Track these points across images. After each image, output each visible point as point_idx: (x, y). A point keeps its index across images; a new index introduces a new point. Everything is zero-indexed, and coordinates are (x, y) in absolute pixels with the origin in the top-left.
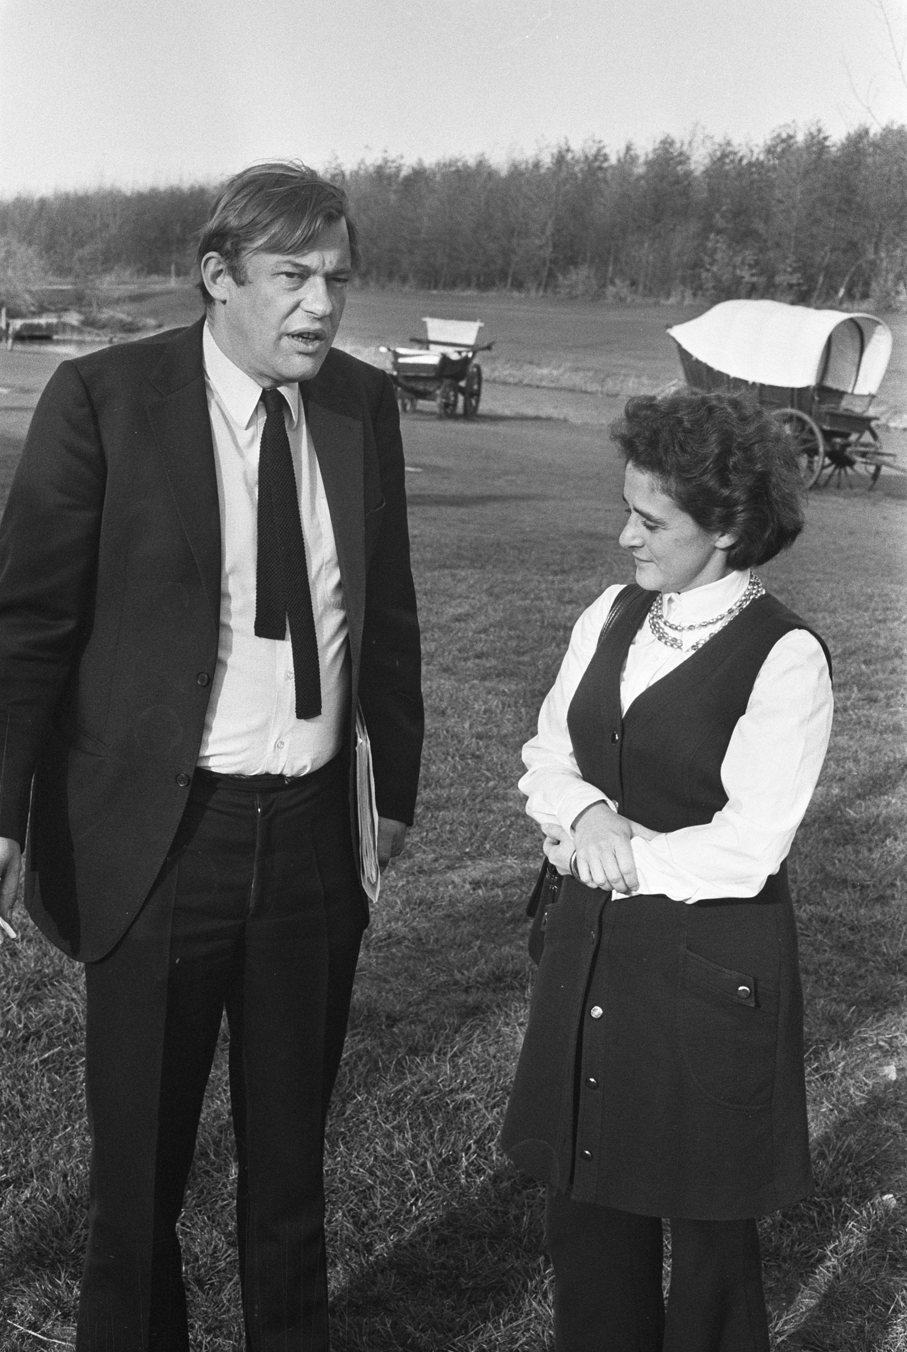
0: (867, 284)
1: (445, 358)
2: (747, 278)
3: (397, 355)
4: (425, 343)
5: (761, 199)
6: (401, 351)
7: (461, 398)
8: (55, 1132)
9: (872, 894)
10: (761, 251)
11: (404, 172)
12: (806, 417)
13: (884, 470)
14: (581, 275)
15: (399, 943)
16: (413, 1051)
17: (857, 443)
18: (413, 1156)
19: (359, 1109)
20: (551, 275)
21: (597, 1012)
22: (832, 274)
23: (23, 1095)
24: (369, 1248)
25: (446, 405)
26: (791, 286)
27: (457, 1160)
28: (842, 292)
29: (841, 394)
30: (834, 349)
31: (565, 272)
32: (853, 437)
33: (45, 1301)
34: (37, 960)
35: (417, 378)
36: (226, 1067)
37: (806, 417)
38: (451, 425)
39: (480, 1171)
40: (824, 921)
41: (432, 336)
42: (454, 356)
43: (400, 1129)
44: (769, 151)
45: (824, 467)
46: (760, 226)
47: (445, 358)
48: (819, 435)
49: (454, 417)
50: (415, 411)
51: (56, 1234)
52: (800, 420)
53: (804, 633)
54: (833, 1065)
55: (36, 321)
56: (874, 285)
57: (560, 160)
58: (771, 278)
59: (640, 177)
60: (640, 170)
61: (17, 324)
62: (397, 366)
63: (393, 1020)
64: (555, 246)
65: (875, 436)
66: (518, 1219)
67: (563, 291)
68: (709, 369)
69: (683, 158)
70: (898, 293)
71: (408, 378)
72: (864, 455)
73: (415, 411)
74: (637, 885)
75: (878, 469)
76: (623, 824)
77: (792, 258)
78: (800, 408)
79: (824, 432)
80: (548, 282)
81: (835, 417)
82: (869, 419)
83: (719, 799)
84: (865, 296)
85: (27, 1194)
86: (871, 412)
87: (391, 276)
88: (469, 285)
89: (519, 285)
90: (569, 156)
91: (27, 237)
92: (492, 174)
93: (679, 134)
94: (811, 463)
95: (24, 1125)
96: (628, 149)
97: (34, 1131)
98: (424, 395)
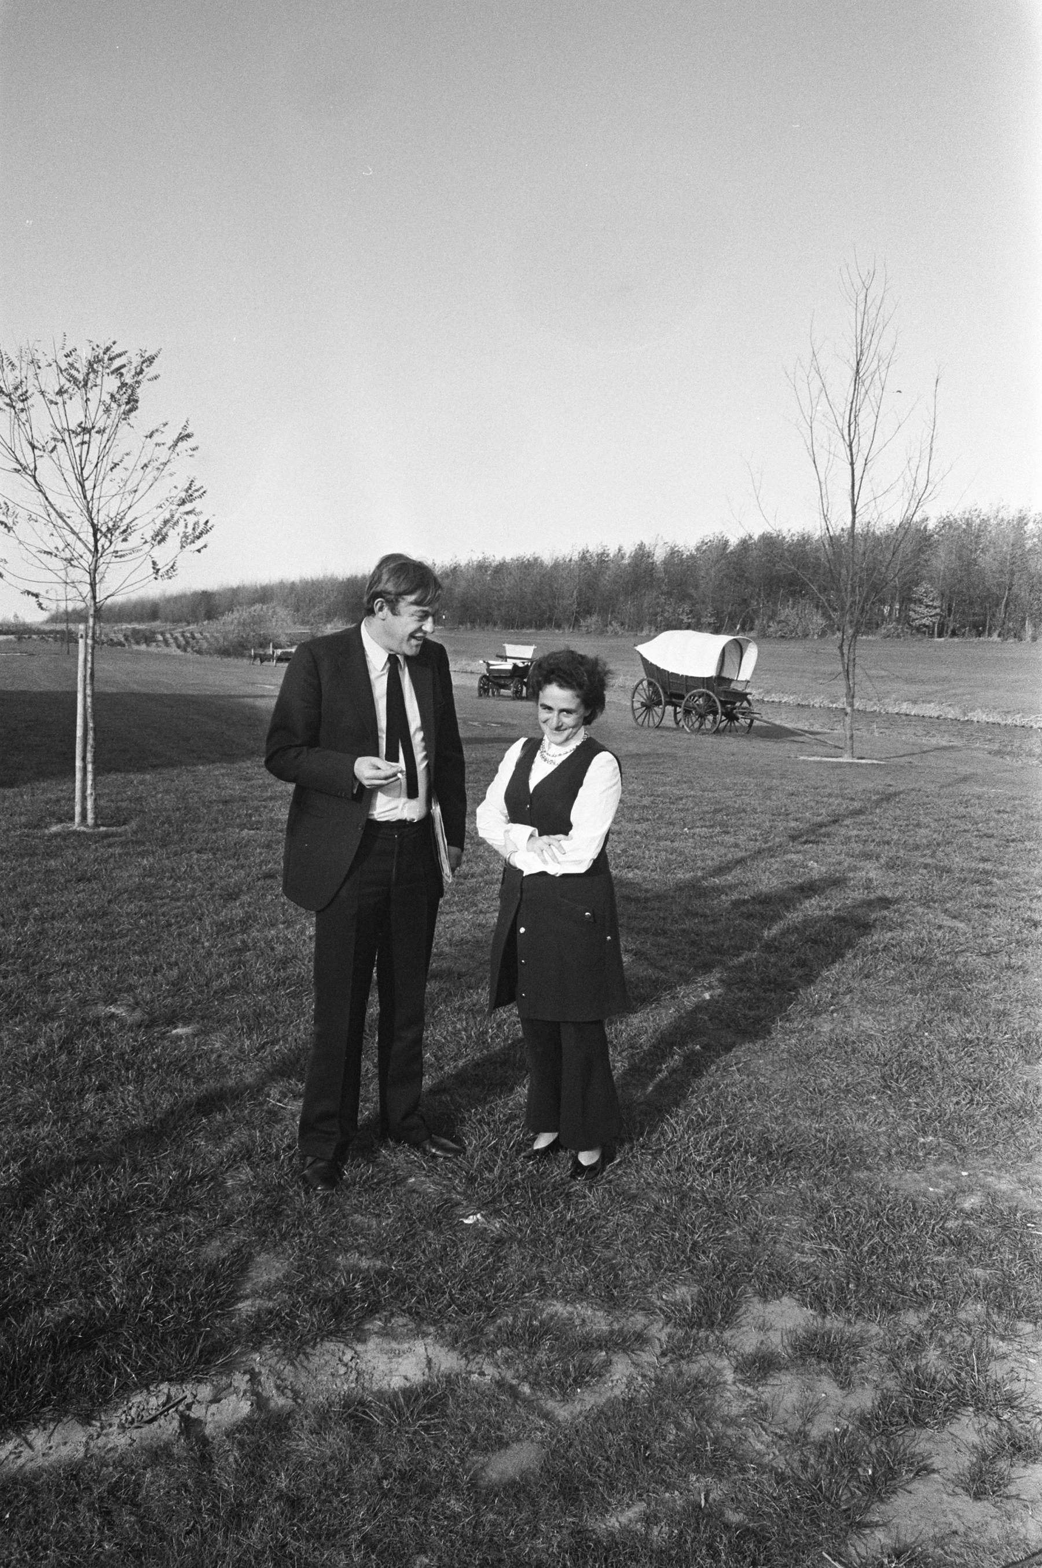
0: (752, 622)
1: (515, 666)
2: (685, 620)
3: (489, 665)
4: (505, 658)
6: (491, 662)
7: (525, 688)
8: (292, 1022)
9: (709, 919)
10: (693, 605)
11: (496, 563)
12: (711, 693)
13: (756, 723)
14: (593, 620)
15: (467, 943)
16: (469, 987)
17: (740, 707)
18: (465, 1030)
19: (441, 1012)
20: (577, 620)
21: (522, 930)
22: (732, 617)
23: (276, 1008)
24: (442, 1068)
25: (516, 692)
26: (710, 624)
27: (487, 1032)
28: (738, 627)
29: (730, 681)
31: (585, 618)
32: (738, 704)
33: (285, 1090)
34: (284, 951)
35: (500, 677)
36: (377, 995)
37: (711, 693)
38: (519, 703)
39: (497, 1037)
40: (684, 931)
41: (508, 654)
42: (521, 665)
43: (460, 1020)
44: (698, 549)
45: (721, 722)
46: (692, 591)
47: (515, 666)
48: (718, 704)
49: (521, 698)
50: (499, 695)
51: (291, 1063)
52: (708, 695)
53: (607, 753)
54: (679, 993)
55: (289, 650)
56: (757, 622)
57: (583, 558)
58: (699, 619)
59: (626, 566)
60: (626, 561)
61: (279, 652)
62: (488, 670)
63: (460, 976)
64: (579, 604)
65: (750, 704)
66: (514, 1056)
67: (584, 629)
68: (658, 668)
69: (649, 555)
70: (769, 627)
71: (495, 677)
72: (743, 714)
73: (499, 695)
75: (752, 722)
77: (710, 609)
78: (708, 688)
79: (721, 701)
80: (575, 624)
82: (747, 694)
83: (570, 826)
84: (751, 629)
85: (277, 1047)
86: (748, 691)
87: (487, 622)
88: (531, 627)
89: (558, 626)
90: (588, 555)
91: (285, 603)
92: (542, 564)
93: (648, 543)
94: (715, 718)
95: (276, 1020)
96: (620, 550)
97: (281, 1022)
98: (505, 687)
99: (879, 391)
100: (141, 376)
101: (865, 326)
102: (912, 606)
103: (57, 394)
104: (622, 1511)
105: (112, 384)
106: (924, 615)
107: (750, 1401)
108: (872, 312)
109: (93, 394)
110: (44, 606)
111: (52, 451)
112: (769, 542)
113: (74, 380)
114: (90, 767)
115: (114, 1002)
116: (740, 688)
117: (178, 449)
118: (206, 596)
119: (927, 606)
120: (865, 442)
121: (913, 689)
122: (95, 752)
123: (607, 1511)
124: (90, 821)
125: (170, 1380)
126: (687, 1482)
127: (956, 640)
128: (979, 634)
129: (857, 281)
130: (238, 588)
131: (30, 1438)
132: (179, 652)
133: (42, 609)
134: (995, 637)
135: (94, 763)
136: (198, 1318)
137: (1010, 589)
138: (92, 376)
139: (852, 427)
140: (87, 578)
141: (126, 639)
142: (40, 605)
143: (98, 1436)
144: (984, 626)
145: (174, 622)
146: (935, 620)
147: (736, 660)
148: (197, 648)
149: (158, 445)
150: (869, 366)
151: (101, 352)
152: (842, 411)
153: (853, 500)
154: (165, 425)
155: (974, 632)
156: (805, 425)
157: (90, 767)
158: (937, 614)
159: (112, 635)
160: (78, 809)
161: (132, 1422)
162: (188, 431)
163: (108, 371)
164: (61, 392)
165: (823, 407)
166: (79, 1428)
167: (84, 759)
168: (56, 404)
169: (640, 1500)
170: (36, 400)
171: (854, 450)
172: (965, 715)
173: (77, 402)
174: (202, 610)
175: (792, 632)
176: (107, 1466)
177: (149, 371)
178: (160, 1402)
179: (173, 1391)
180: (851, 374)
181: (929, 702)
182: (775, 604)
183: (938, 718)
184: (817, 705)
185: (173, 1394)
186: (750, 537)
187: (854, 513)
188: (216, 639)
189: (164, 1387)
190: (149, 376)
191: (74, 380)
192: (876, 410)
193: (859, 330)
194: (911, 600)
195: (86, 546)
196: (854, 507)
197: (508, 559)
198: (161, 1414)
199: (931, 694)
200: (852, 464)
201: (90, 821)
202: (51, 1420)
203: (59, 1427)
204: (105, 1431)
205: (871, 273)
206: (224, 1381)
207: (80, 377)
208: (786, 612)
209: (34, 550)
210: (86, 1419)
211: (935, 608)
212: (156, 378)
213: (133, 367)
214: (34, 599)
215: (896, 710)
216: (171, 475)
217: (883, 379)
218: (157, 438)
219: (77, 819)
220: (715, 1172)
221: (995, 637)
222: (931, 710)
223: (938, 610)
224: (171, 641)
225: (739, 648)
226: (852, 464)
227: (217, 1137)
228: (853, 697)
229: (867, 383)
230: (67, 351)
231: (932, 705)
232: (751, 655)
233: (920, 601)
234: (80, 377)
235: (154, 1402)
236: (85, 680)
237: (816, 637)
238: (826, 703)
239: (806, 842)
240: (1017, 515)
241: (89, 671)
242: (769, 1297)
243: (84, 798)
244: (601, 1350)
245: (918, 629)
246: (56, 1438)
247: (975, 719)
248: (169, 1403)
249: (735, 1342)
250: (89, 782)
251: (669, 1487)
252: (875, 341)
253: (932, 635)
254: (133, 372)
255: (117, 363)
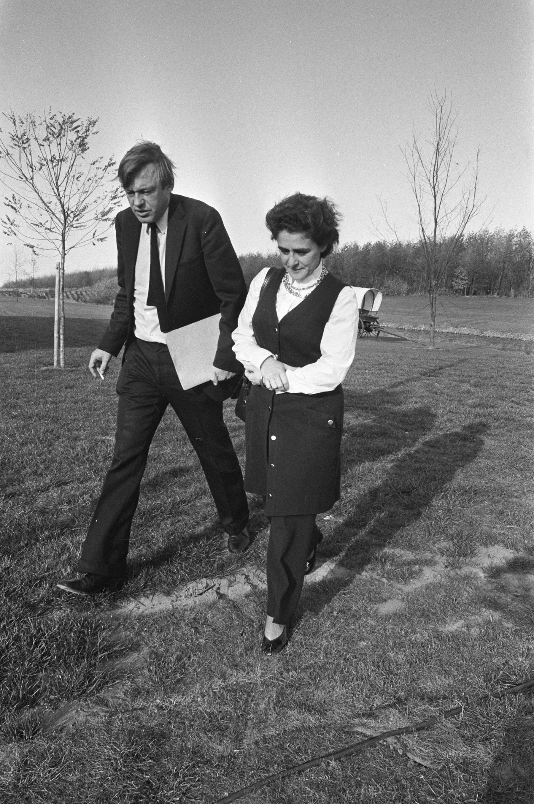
5: (341, 264)
29: (368, 311)
30: (366, 299)
32: (372, 323)
46: (341, 271)
65: (377, 323)
72: (375, 328)
74: (288, 389)
76: (280, 364)
81: (367, 317)
86: (377, 316)
99: (449, 158)
100: (88, 133)
101: (441, 125)
102: (454, 279)
103: (44, 140)
104: (453, 624)
105: (72, 136)
106: (461, 284)
107: (495, 584)
108: (445, 117)
109: (63, 141)
110: (36, 253)
111: (40, 170)
112: (380, 247)
113: (53, 134)
114: (62, 337)
115: (107, 434)
116: (373, 315)
117: (108, 170)
118: (87, 273)
119: (461, 279)
120: (441, 186)
121: (455, 320)
122: (64, 329)
123: (446, 623)
124: (62, 365)
125: (206, 577)
126: (481, 612)
127: (476, 296)
128: (488, 293)
129: (437, 104)
130: (103, 270)
131: (142, 601)
132: (74, 302)
133: (35, 254)
134: (495, 295)
135: (64, 334)
136: (208, 555)
137: (503, 271)
138: (63, 131)
139: (435, 178)
140: (60, 238)
141: (47, 295)
142: (34, 252)
143: (177, 601)
144: (490, 289)
145: (70, 287)
146: (466, 286)
147: (371, 302)
148: (84, 299)
149: (98, 168)
150: (444, 145)
151: (67, 118)
152: (429, 169)
153: (435, 215)
154: (101, 158)
155: (485, 292)
156: (411, 176)
157: (62, 337)
158: (467, 283)
159: (40, 294)
160: (55, 358)
161: (191, 595)
162: (113, 161)
163: (70, 129)
164: (47, 139)
165: (420, 168)
166: (165, 598)
167: (59, 332)
168: (43, 146)
169: (461, 619)
170: (32, 142)
171: (436, 190)
172: (482, 333)
173: (54, 145)
174: (84, 281)
175: (392, 292)
176: (187, 611)
177: (93, 129)
178: (204, 586)
179: (209, 581)
180: (434, 149)
181: (464, 327)
182: (383, 278)
183: (468, 334)
184: (406, 328)
185: (209, 583)
186: (370, 244)
187: (436, 222)
188: (94, 295)
189: (204, 580)
190: (93, 132)
191: (53, 134)
192: (447, 168)
193: (438, 126)
194: (454, 276)
195: (60, 221)
196: (436, 219)
197: (244, 255)
198: (205, 592)
199: (464, 323)
200: (435, 197)
201: (62, 365)
202: (149, 594)
203: (155, 597)
204: (179, 599)
205: (444, 98)
206: (232, 578)
207: (56, 131)
208: (388, 282)
209: (29, 222)
210: (168, 594)
211: (465, 280)
212: (97, 133)
213: (84, 127)
214: (31, 249)
215: (447, 331)
216: (102, 186)
217: (451, 152)
218: (97, 165)
219: (55, 364)
220: (442, 498)
221: (495, 295)
222: (465, 330)
223: (467, 281)
224: (70, 296)
225: (372, 295)
226: (435, 197)
227: (184, 486)
228: (435, 316)
229: (443, 154)
230: (51, 116)
231: (465, 328)
232: (379, 298)
233: (458, 277)
234: (56, 131)
235: (200, 586)
236: (59, 291)
237: (404, 295)
238: (411, 327)
239: (429, 376)
240: (509, 233)
241: (61, 287)
242: (489, 545)
243: (59, 355)
244: (416, 565)
245: (456, 291)
246: (155, 602)
247: (487, 335)
248: (208, 588)
249: (479, 562)
250: (62, 345)
251: (474, 614)
252: (446, 134)
253: (463, 294)
254: (84, 130)
255: (75, 125)
